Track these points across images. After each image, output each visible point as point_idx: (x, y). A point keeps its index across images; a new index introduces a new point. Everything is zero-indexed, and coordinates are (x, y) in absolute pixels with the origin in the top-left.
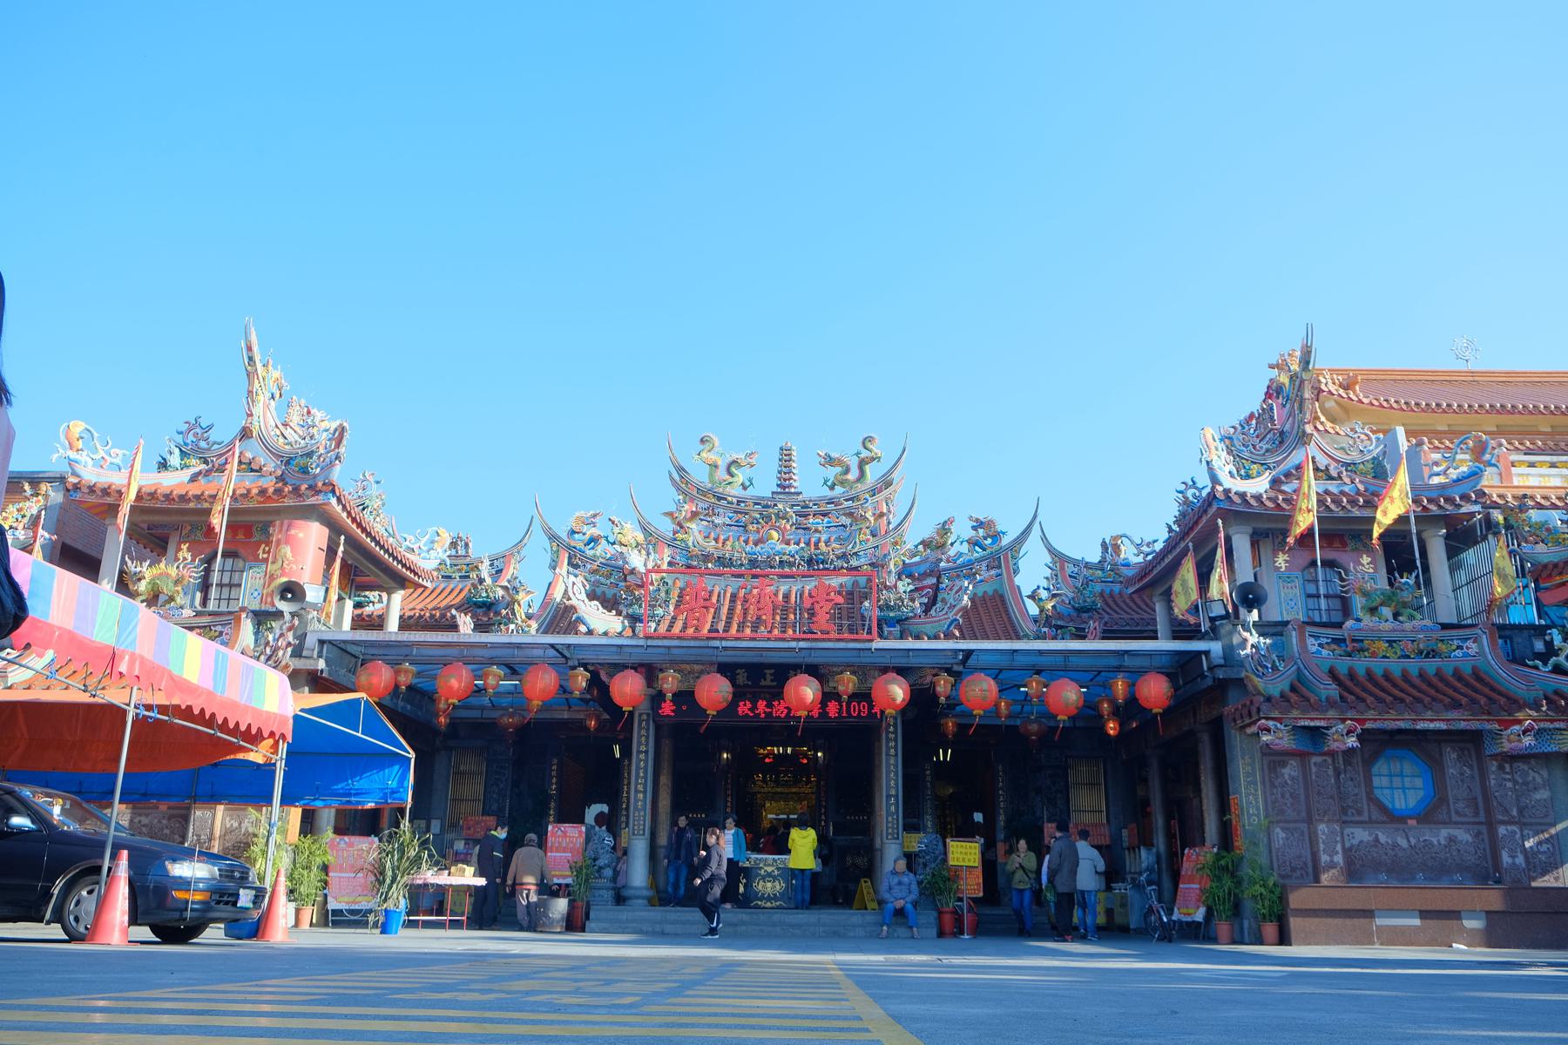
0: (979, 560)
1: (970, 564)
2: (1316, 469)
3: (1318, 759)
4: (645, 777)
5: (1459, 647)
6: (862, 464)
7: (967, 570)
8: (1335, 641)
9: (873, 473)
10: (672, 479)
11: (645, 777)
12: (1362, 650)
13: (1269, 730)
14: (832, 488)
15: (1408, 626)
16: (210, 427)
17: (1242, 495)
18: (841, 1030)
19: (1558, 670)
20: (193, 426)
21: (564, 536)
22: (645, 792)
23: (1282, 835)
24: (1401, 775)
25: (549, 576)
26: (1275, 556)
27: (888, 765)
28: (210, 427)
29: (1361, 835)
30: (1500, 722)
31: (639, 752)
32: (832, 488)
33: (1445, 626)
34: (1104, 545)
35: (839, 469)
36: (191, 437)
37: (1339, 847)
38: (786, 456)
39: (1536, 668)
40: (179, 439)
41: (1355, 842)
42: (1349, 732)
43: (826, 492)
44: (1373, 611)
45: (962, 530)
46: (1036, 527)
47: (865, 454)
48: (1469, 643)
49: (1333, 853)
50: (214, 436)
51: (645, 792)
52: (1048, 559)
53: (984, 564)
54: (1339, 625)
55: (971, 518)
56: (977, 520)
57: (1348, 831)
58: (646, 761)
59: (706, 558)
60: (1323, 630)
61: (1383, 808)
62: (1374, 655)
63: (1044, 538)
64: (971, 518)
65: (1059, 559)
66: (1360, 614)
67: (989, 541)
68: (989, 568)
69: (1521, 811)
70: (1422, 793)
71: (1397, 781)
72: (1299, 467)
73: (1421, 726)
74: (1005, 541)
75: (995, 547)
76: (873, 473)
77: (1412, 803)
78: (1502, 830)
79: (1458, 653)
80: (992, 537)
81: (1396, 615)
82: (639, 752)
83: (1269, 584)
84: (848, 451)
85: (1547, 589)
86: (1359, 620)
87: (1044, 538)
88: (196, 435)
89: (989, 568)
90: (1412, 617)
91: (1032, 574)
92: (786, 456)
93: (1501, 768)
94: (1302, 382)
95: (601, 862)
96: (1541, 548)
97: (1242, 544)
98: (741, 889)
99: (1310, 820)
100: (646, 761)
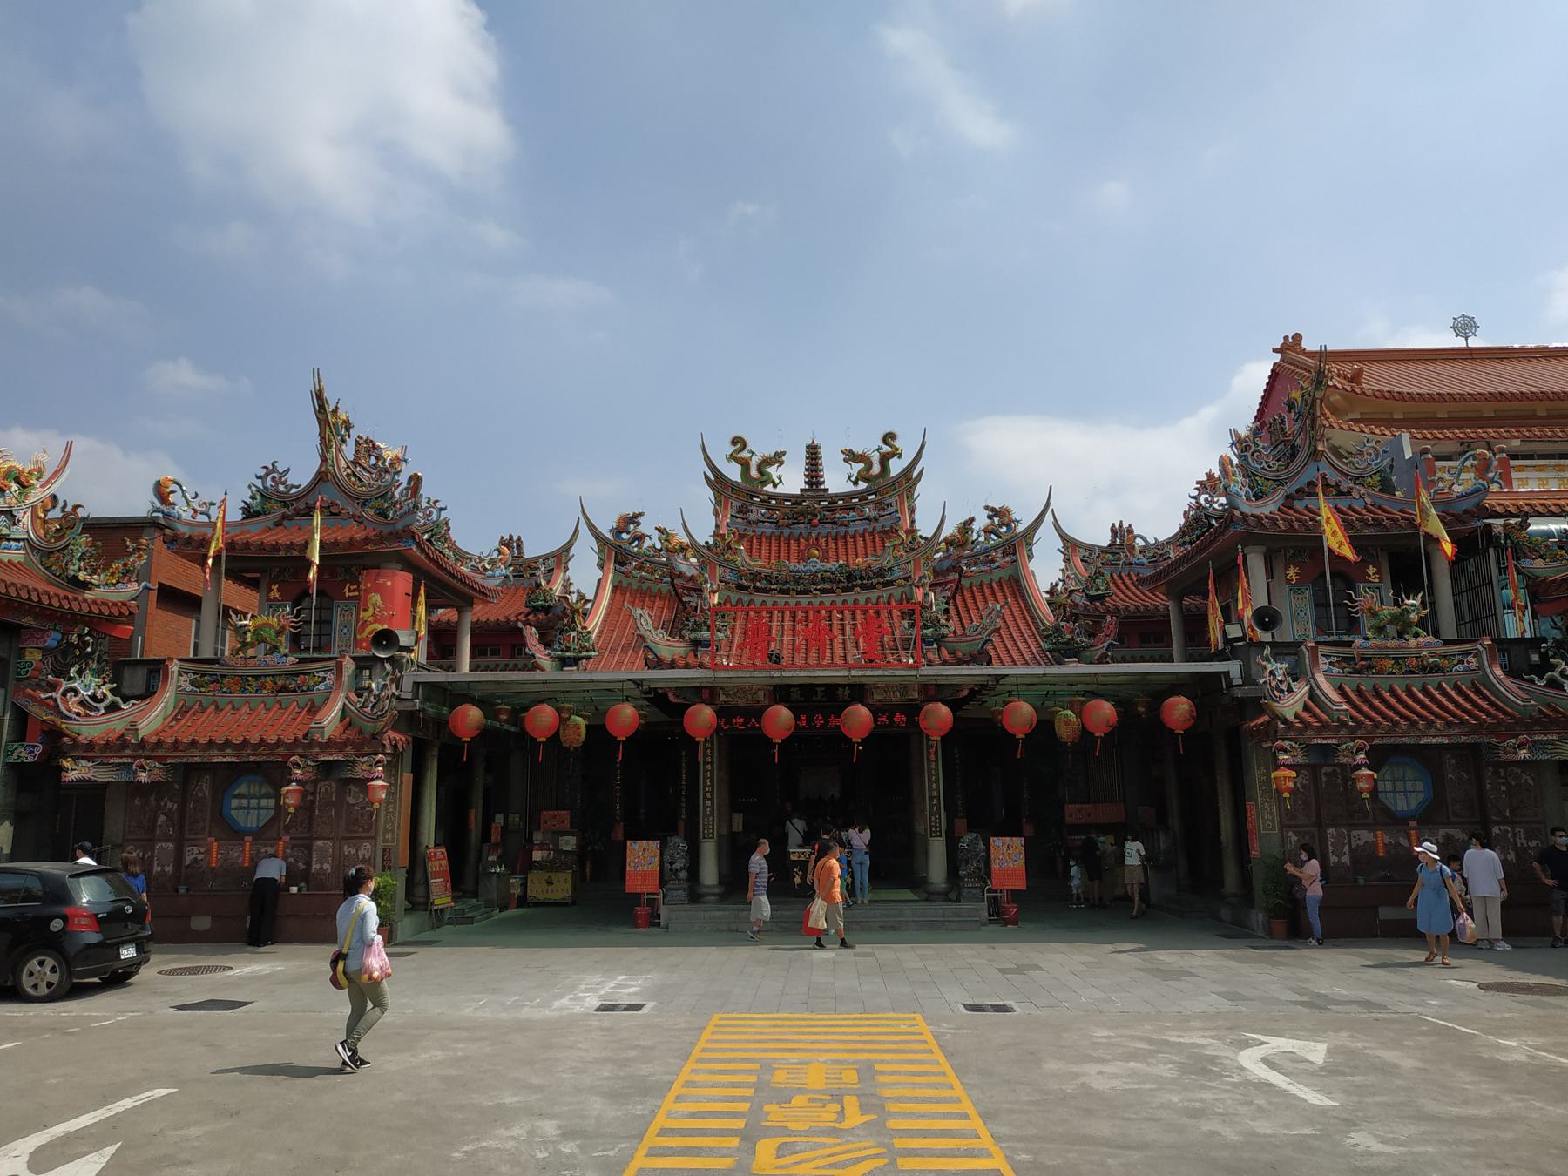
0: (996, 547)
1: (987, 551)
2: (1326, 485)
3: (1329, 770)
4: (712, 786)
5: (1461, 662)
6: (884, 459)
7: (986, 557)
8: (1344, 659)
9: (896, 466)
10: (706, 477)
11: (712, 786)
12: (1370, 667)
13: (1285, 751)
14: (856, 483)
15: (1413, 642)
16: (287, 471)
17: (1258, 518)
18: (924, 1100)
19: (1554, 684)
20: (270, 470)
21: (609, 536)
22: (712, 799)
23: (1295, 838)
24: (1404, 780)
25: (599, 574)
26: (1287, 569)
27: (930, 769)
28: (287, 471)
29: (1365, 836)
30: (1497, 736)
31: (706, 763)
32: (856, 483)
33: (1447, 643)
34: (1114, 531)
35: (862, 465)
36: (269, 482)
37: (1346, 849)
38: (813, 452)
39: (1532, 681)
40: (259, 483)
41: (1361, 843)
42: (1359, 750)
43: (850, 488)
44: (1380, 630)
45: (981, 522)
46: (1049, 515)
47: (886, 449)
48: (1470, 658)
49: (1340, 854)
50: (291, 479)
51: (712, 799)
52: (1060, 545)
53: (1000, 551)
54: (1349, 644)
55: (987, 508)
56: (993, 509)
57: (1354, 833)
58: (712, 771)
59: (755, 576)
60: (1333, 649)
61: (1386, 810)
62: (1381, 672)
63: (1056, 525)
64: (987, 508)
65: (1070, 545)
66: (1369, 634)
67: (1004, 529)
68: (1005, 554)
69: (1512, 812)
70: (1421, 796)
71: (1399, 785)
72: (1311, 484)
73: (1424, 741)
74: (1020, 528)
75: (1011, 535)
76: (896, 466)
77: (1413, 805)
78: (1495, 830)
79: (1460, 667)
80: (1008, 525)
81: (1400, 635)
82: (706, 763)
83: (1283, 606)
84: (870, 445)
85: (1545, 602)
86: (1367, 639)
87: (1056, 525)
88: (273, 479)
89: (1005, 554)
90: (1417, 635)
91: (1046, 569)
92: (813, 452)
93: (1496, 773)
94: (1314, 400)
95: (677, 866)
96: (1539, 563)
97: (1256, 563)
98: (797, 880)
99: (1320, 825)
100: (712, 771)
